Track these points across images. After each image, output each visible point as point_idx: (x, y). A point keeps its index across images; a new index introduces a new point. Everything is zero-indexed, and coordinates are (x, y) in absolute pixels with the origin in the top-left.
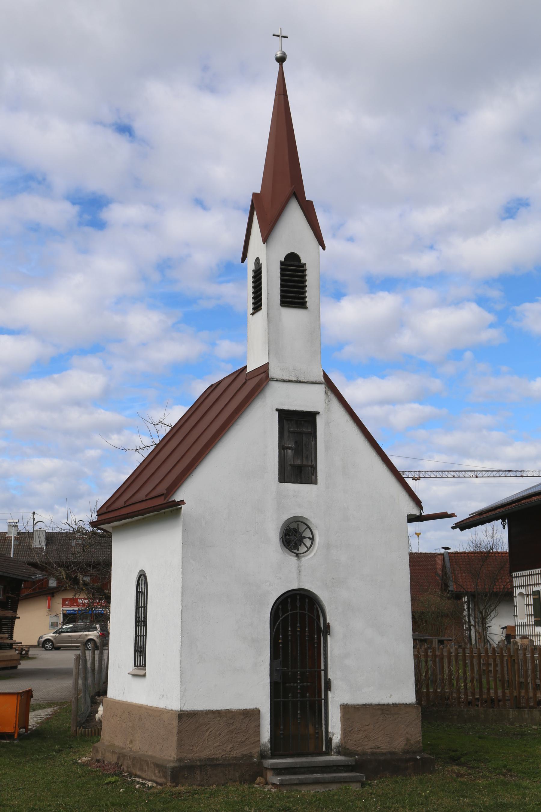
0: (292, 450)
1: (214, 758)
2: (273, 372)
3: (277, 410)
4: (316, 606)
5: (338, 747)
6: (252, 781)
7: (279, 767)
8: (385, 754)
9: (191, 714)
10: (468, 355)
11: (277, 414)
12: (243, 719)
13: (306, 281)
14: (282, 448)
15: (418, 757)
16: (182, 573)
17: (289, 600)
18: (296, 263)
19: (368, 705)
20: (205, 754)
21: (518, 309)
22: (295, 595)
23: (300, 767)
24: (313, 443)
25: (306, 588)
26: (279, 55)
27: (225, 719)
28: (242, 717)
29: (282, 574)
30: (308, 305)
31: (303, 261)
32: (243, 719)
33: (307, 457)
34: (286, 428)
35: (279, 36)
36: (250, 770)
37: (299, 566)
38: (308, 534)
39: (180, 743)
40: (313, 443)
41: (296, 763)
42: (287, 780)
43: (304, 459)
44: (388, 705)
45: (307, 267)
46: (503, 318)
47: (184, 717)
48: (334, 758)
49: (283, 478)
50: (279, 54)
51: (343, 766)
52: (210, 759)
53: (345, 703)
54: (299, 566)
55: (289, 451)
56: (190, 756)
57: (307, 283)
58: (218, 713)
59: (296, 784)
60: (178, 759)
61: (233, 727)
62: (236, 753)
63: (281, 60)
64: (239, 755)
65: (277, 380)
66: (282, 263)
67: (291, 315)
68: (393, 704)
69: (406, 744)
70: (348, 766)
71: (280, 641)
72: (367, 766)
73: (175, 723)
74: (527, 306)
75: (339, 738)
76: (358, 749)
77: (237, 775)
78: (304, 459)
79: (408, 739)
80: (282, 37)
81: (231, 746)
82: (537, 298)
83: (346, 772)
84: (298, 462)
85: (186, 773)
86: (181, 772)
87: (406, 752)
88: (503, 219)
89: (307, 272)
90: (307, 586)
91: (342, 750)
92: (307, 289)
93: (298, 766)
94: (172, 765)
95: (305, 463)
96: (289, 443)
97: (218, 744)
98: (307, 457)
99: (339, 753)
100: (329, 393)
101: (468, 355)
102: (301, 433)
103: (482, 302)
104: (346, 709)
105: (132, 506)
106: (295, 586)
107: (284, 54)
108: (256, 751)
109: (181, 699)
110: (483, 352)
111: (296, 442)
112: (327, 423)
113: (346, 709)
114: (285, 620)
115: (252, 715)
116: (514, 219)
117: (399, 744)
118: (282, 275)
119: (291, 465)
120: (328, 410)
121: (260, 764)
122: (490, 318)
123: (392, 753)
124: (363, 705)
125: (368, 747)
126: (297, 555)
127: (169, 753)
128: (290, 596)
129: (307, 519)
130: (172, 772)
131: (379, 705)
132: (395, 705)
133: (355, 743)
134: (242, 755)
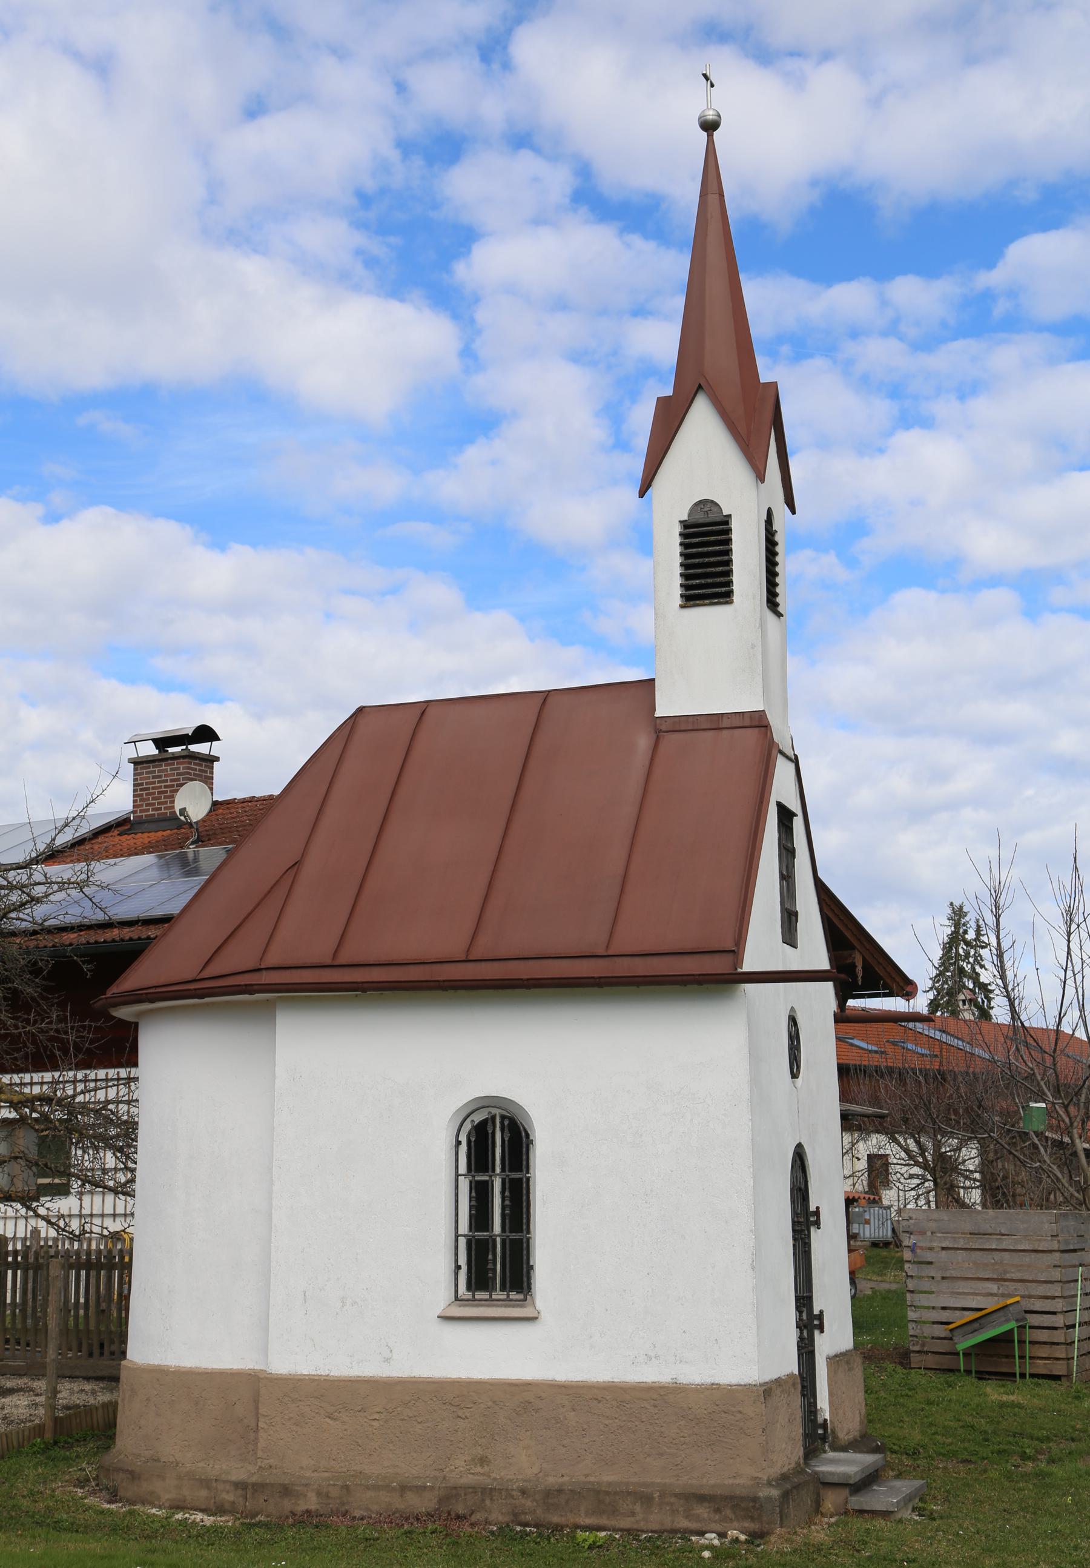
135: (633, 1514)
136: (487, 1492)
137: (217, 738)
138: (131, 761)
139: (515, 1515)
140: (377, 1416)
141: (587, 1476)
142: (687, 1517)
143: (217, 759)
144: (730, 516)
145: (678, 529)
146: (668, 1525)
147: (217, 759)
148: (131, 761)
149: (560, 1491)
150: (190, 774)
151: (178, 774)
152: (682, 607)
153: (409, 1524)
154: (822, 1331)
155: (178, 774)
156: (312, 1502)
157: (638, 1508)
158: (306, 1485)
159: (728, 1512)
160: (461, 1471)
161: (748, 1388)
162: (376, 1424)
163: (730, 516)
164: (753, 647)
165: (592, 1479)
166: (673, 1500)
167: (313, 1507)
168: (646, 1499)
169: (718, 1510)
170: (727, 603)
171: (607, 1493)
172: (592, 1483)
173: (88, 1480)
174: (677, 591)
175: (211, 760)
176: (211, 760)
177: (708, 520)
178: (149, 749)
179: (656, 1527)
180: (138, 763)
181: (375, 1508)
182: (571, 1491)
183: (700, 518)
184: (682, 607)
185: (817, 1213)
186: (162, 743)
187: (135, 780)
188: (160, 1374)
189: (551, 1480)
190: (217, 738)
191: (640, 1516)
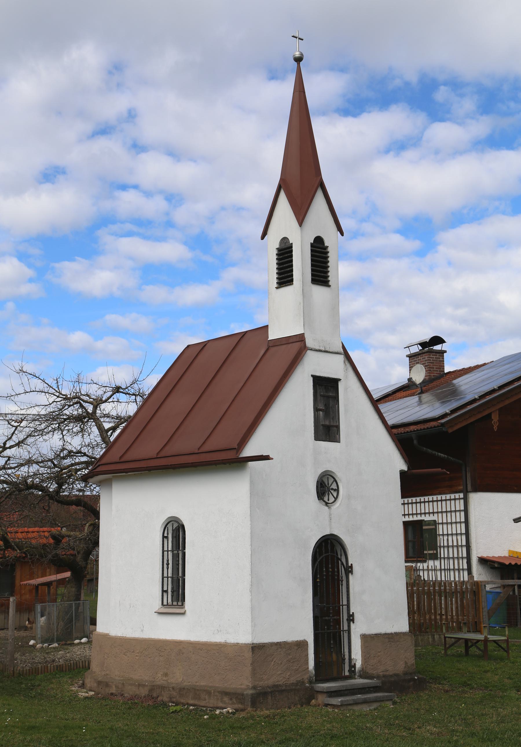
0: (323, 412)
1: (277, 685)
2: (309, 343)
3: (312, 376)
4: (339, 549)
5: (360, 671)
6: (308, 703)
7: (332, 690)
8: (391, 676)
9: (261, 646)
10: (10, 305)
11: (312, 379)
12: (297, 649)
13: (328, 262)
14: (316, 410)
15: (416, 678)
16: (251, 520)
17: (323, 544)
18: (321, 246)
19: (379, 634)
20: (271, 682)
21: (57, 265)
22: (328, 539)
23: (346, 690)
24: (337, 406)
25: (335, 534)
26: (297, 56)
27: (284, 650)
28: (296, 648)
29: (315, 522)
30: (330, 283)
31: (326, 244)
32: (297, 649)
33: (333, 419)
34: (318, 391)
35: (296, 38)
36: (305, 694)
37: (330, 515)
38: (334, 486)
39: (254, 672)
40: (337, 406)
41: (343, 686)
42: (345, 701)
43: (331, 420)
44: (391, 634)
45: (329, 249)
46: (40, 274)
47: (256, 648)
48: (359, 681)
49: (317, 438)
50: (297, 54)
51: (373, 687)
52: (275, 686)
53: (364, 633)
54: (330, 515)
55: (321, 413)
56: (261, 683)
57: (329, 264)
58: (279, 645)
59: (350, 705)
60: (252, 687)
61: (290, 657)
62: (293, 680)
63: (298, 60)
64: (295, 682)
65: (311, 350)
66: (312, 245)
67: (318, 290)
68: (395, 633)
69: (405, 667)
70: (377, 687)
71: (318, 580)
72: (396, 685)
73: (249, 654)
74: (66, 264)
75: (360, 663)
76: (374, 672)
77: (297, 698)
78: (331, 420)
79: (406, 663)
80: (299, 39)
81: (289, 674)
82: (76, 258)
83: (375, 692)
84: (327, 423)
85: (261, 699)
86: (260, 697)
87: (405, 674)
88: (41, 183)
89: (329, 254)
90: (335, 533)
91: (364, 674)
92: (329, 269)
93: (344, 689)
94: (251, 692)
95: (332, 424)
96: (321, 406)
97: (280, 672)
98: (333, 419)
99: (361, 677)
100: (347, 362)
101: (10, 305)
102: (328, 397)
103: (22, 257)
104: (365, 638)
105: (176, 457)
106: (328, 532)
107: (302, 54)
108: (306, 677)
109: (252, 633)
110: (23, 304)
111: (325, 405)
112: (346, 389)
113: (365, 638)
114: (321, 562)
115: (302, 645)
116: (53, 183)
117: (400, 668)
118: (312, 256)
119: (322, 425)
120: (346, 377)
121: (312, 688)
122: (29, 273)
123: (397, 675)
124: (376, 634)
125: (380, 670)
126: (327, 504)
127: (243, 681)
128: (323, 541)
129: (334, 473)
130: (252, 698)
131: (386, 634)
132: (396, 634)
133: (372, 667)
134: (297, 681)
135: (205, 700)
136: (163, 688)
137: (444, 342)
138: (407, 356)
139: (171, 698)
140: (137, 655)
141: (196, 682)
142: (221, 702)
143: (445, 352)
144: (292, 244)
145: (276, 252)
146: (215, 705)
147: (445, 352)
148: (407, 356)
149: (184, 688)
150: (430, 360)
151: (425, 361)
152: (277, 288)
153: (133, 702)
154: (353, 623)
155: (425, 361)
156: (113, 690)
157: (207, 697)
158: (112, 682)
159: (234, 700)
160: (160, 680)
161: (246, 645)
162: (137, 658)
163: (292, 244)
164: (300, 304)
165: (198, 684)
166: (217, 694)
167: (114, 692)
168: (209, 693)
169: (231, 699)
170: (290, 285)
171: (198, 690)
172: (198, 686)
173: (319, 706)
174: (276, 281)
175: (443, 352)
176: (443, 352)
177: (286, 247)
178: (416, 349)
179: (212, 706)
180: (411, 357)
181: (131, 693)
182: (188, 689)
183: (284, 246)
184: (277, 288)
185: (351, 566)
186: (424, 345)
187: (410, 365)
188: (106, 637)
189: (185, 684)
190: (444, 342)
191: (207, 701)
